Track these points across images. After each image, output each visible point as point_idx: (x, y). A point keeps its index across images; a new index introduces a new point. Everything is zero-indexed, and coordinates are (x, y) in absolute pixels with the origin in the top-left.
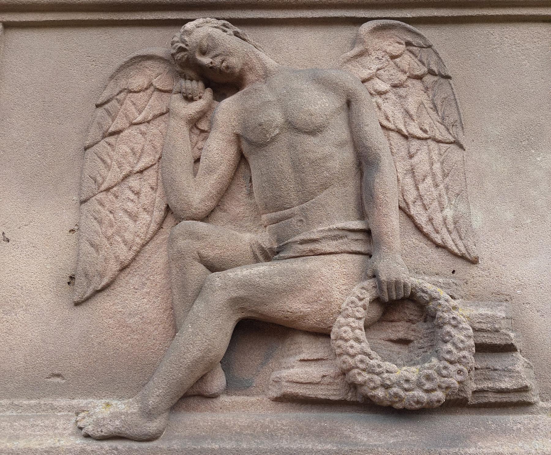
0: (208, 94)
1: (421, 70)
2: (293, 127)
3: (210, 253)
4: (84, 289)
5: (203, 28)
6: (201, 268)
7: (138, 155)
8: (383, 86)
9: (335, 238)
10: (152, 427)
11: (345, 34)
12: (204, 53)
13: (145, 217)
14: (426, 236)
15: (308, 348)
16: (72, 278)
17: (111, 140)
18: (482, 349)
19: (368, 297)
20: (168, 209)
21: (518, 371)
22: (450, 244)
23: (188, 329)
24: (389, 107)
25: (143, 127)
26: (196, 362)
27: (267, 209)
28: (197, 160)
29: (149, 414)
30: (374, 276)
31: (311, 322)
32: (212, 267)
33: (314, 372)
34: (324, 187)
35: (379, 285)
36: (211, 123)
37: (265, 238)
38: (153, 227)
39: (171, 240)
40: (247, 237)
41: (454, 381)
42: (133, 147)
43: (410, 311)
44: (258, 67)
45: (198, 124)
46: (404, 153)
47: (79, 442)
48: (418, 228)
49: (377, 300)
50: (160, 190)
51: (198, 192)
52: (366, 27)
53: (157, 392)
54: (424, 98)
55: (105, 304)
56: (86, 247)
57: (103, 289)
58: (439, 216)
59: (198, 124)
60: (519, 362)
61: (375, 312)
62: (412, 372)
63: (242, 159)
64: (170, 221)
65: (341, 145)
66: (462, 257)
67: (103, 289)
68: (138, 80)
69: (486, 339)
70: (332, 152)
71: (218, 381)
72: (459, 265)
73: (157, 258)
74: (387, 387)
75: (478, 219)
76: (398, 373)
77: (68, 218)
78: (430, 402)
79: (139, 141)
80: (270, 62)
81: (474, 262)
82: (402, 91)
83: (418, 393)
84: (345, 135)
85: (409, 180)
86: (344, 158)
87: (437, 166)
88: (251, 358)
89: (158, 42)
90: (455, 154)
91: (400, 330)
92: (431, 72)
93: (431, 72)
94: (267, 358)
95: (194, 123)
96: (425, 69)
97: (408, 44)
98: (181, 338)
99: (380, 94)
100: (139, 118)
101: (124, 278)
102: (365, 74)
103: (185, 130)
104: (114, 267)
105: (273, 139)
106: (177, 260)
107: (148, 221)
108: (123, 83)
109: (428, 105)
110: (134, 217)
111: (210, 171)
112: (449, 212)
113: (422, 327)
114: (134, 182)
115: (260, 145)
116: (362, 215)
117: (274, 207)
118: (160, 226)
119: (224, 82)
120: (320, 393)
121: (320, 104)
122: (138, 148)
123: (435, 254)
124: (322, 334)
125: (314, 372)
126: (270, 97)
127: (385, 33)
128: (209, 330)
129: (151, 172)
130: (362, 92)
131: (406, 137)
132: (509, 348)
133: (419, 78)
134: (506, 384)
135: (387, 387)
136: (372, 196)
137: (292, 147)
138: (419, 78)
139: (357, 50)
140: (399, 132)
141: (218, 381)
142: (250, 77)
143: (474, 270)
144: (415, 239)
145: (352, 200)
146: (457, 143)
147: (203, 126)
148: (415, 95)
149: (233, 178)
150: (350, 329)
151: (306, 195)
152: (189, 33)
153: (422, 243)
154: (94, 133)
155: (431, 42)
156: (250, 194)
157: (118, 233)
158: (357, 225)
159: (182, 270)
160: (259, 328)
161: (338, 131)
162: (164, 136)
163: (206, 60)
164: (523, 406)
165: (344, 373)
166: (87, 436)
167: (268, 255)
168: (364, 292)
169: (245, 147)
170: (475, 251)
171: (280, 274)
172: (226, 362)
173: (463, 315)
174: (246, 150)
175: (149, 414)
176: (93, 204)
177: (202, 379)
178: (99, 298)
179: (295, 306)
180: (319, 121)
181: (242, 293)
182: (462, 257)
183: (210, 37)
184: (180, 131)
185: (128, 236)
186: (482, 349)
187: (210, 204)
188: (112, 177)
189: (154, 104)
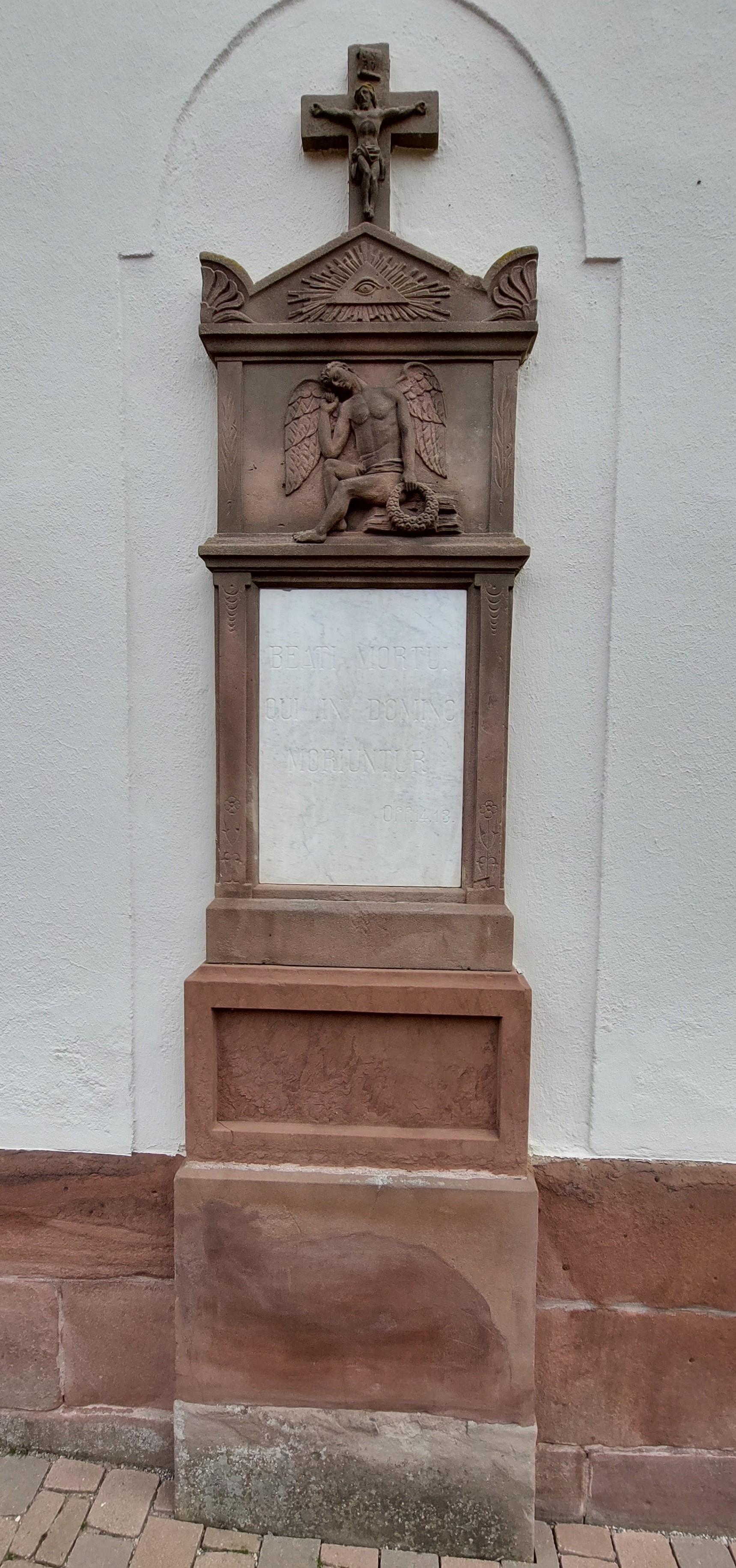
0: (337, 400)
1: (429, 388)
2: (373, 416)
3: (340, 473)
4: (289, 489)
5: (334, 367)
6: (335, 479)
7: (308, 429)
8: (413, 396)
9: (389, 465)
10: (322, 537)
11: (397, 368)
12: (335, 380)
13: (312, 458)
14: (427, 467)
15: (378, 512)
16: (284, 485)
17: (296, 421)
18: (442, 512)
19: (400, 489)
20: (321, 455)
21: (455, 519)
22: (436, 470)
23: (332, 503)
24: (415, 406)
25: (309, 415)
26: (337, 514)
27: (362, 454)
28: (333, 431)
29: (320, 533)
30: (403, 481)
31: (379, 500)
32: (340, 479)
33: (380, 520)
34: (385, 443)
35: (404, 486)
36: (338, 415)
37: (361, 467)
38: (316, 462)
39: (324, 467)
40: (354, 466)
41: (429, 520)
42: (305, 425)
43: (417, 497)
44: (358, 386)
45: (333, 414)
46: (420, 428)
47: (296, 544)
48: (424, 463)
49: (404, 492)
50: (318, 445)
51: (334, 446)
52: (409, 364)
53: (323, 525)
54: (430, 402)
55: (298, 496)
56: (289, 471)
57: (298, 489)
58: (432, 457)
59: (333, 414)
60: (455, 517)
61: (403, 496)
62: (415, 518)
63: (351, 432)
64: (322, 458)
65: (393, 424)
66: (441, 476)
67: (298, 489)
68: (306, 392)
69: (444, 507)
70: (388, 427)
71: (344, 525)
72: (440, 479)
73: (318, 476)
74: (405, 523)
76: (408, 518)
77: (280, 458)
78: (420, 528)
79: (308, 423)
80: (364, 384)
81: (445, 478)
82: (421, 398)
83: (416, 525)
84: (395, 420)
85: (422, 441)
86: (395, 428)
87: (434, 434)
88: (356, 518)
89: (311, 372)
90: (442, 430)
91: (413, 505)
92: (434, 389)
93: (434, 389)
94: (363, 517)
95: (331, 413)
96: (431, 388)
97: (425, 374)
98: (329, 506)
99: (412, 399)
100: (308, 411)
101: (304, 485)
102: (405, 389)
103: (328, 416)
104: (301, 480)
105: (365, 421)
106: (326, 476)
107: (313, 459)
108: (300, 394)
109: (432, 405)
110: (307, 457)
111: (339, 436)
112: (437, 456)
113: (421, 503)
114: (306, 441)
115: (360, 424)
116: (401, 456)
117: (365, 453)
118: (318, 462)
119: (344, 393)
120: (382, 528)
121: (384, 405)
122: (308, 426)
123: (431, 475)
124: (383, 505)
125: (380, 520)
126: (364, 402)
127: (415, 369)
128: (340, 503)
129: (314, 437)
130: (403, 400)
131: (422, 421)
132: (453, 512)
133: (429, 391)
134: (450, 524)
135: (405, 523)
136: (404, 447)
137: (372, 425)
138: (429, 391)
139: (403, 377)
140: (419, 418)
141: (344, 525)
142: (355, 391)
143: (446, 482)
144: (423, 468)
145: (397, 451)
146: (442, 424)
147: (335, 415)
148: (427, 400)
149: (348, 439)
150: (393, 503)
151: (378, 447)
152: (328, 370)
153: (426, 470)
154: (289, 419)
155: (435, 374)
156: (355, 447)
157: (301, 464)
158: (398, 460)
159: (329, 480)
160: (361, 504)
161: (392, 418)
162: (319, 420)
163: (336, 384)
164: (456, 533)
165: (391, 518)
166: (299, 542)
167: (363, 473)
168: (399, 488)
169: (353, 425)
170: (445, 473)
171: (367, 480)
172: (347, 517)
173: (435, 498)
174: (354, 424)
175: (320, 533)
176: (290, 452)
177: (338, 523)
178: (295, 493)
179: (373, 493)
180: (383, 413)
181: (352, 488)
182: (441, 476)
183: (338, 372)
184: (325, 416)
185: (306, 466)
186: (442, 512)
187: (339, 451)
188: (297, 439)
189: (314, 404)
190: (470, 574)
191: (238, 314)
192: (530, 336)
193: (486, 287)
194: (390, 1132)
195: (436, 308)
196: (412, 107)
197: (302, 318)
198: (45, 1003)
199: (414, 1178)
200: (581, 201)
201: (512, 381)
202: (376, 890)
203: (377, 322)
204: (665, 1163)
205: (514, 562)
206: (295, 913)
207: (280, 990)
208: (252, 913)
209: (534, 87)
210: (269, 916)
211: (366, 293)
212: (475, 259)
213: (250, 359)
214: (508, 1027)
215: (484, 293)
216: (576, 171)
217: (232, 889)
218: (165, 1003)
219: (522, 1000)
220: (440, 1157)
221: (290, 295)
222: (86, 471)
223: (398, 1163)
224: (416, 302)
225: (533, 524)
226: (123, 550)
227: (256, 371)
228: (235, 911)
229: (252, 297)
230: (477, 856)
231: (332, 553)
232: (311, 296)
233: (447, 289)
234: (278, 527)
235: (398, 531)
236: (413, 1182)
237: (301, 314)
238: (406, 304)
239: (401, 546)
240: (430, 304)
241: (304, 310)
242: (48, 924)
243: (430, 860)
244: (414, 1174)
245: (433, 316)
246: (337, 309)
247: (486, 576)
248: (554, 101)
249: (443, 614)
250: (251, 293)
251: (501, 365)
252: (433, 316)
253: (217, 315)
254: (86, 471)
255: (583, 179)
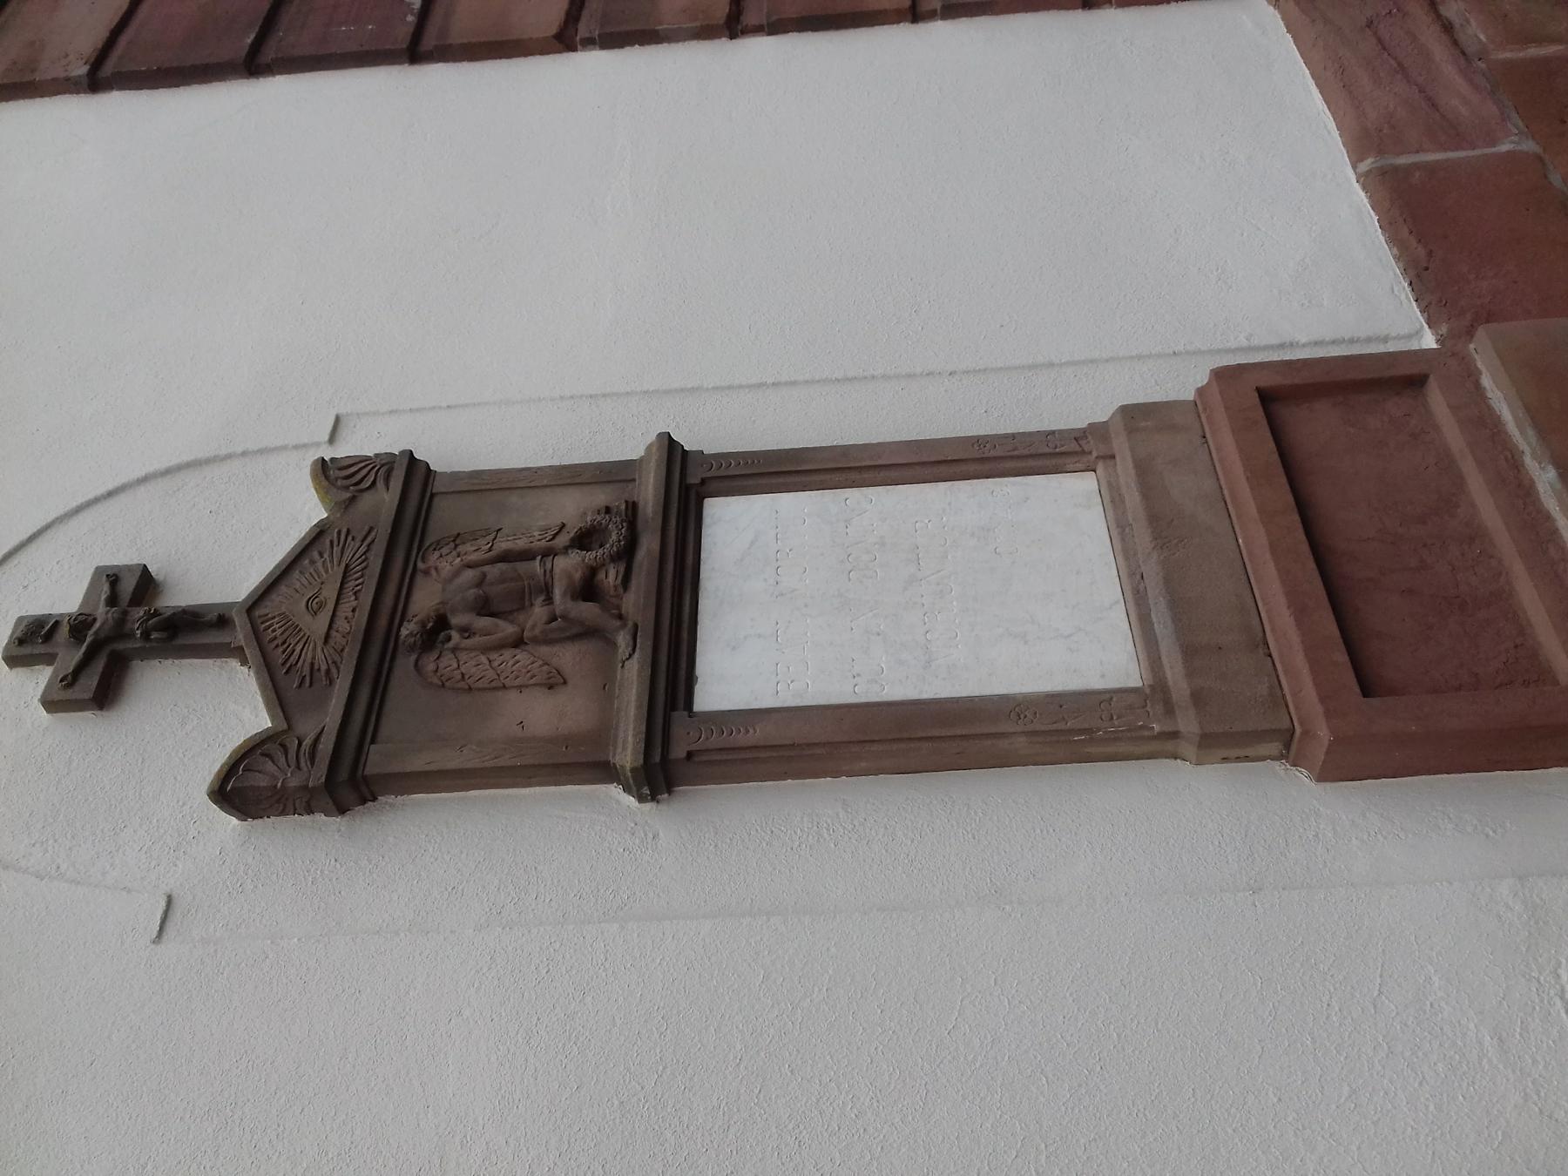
4: (554, 682)
11: (419, 578)
15: (601, 575)
27: (522, 599)
42: (475, 666)
47: (636, 655)
52: (420, 565)
73: (544, 650)
75: (542, 523)
76: (615, 537)
77: (513, 695)
81: (564, 525)
89: (405, 663)
90: (505, 531)
116: (534, 558)
120: (622, 570)
128: (588, 611)
150: (590, 556)
160: (588, 589)
161: (486, 568)
174: (484, 607)
175: (624, 626)
179: (578, 576)
190: (685, 489)
191: (307, 742)
192: (411, 459)
193: (349, 495)
194: (1476, 484)
195: (359, 538)
196: (106, 588)
197: (334, 670)
198: (1480, 1043)
199: (1529, 444)
200: (263, 451)
201: (455, 476)
202: (1118, 546)
203: (361, 596)
204: (1405, 271)
205: (671, 450)
206: (1177, 619)
207: (1300, 612)
208: (1190, 673)
209: (122, 499)
210: (1190, 652)
211: (321, 605)
212: (310, 510)
213: (370, 732)
214: (1268, 381)
215: (353, 499)
216: (229, 457)
217: (1160, 708)
218: (1402, 835)
219: (1225, 376)
220: (1483, 425)
221: (300, 685)
222: (478, 989)
223: (1516, 464)
224: (348, 553)
225: (626, 440)
226: (616, 926)
227: (384, 731)
228: (1192, 694)
229: (290, 727)
230: (1047, 450)
231: (651, 613)
232: (309, 661)
233: (339, 533)
234: (606, 687)
235: (627, 553)
236: (1533, 440)
237: (328, 671)
238: (347, 566)
239: (649, 545)
240: (352, 546)
241: (324, 667)
242: (1314, 1041)
243: (1071, 506)
244: (1523, 445)
245: (369, 539)
246: (333, 633)
247: (691, 478)
248: (145, 480)
249: (729, 523)
250: (285, 726)
251: (438, 486)
252: (369, 539)
253: (303, 764)
254: (478, 989)
255: (240, 450)
